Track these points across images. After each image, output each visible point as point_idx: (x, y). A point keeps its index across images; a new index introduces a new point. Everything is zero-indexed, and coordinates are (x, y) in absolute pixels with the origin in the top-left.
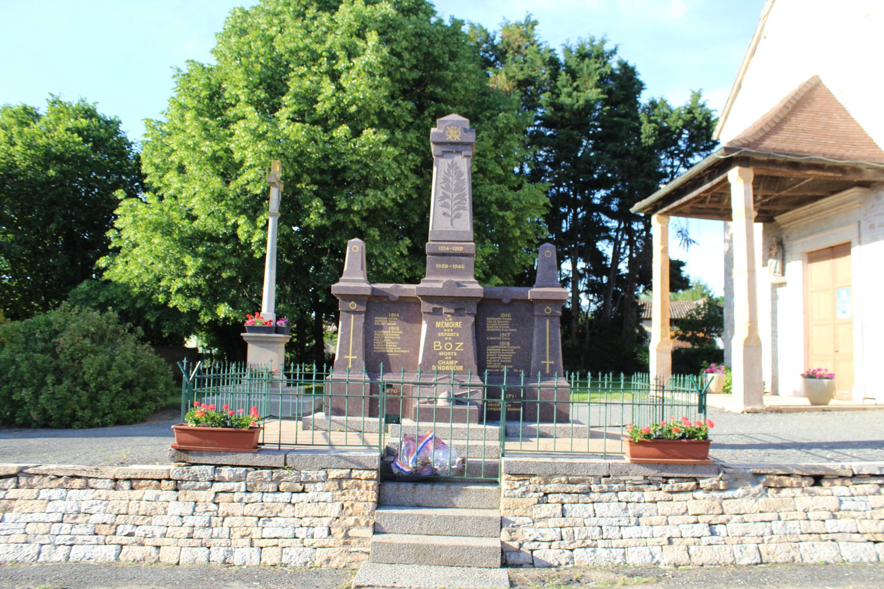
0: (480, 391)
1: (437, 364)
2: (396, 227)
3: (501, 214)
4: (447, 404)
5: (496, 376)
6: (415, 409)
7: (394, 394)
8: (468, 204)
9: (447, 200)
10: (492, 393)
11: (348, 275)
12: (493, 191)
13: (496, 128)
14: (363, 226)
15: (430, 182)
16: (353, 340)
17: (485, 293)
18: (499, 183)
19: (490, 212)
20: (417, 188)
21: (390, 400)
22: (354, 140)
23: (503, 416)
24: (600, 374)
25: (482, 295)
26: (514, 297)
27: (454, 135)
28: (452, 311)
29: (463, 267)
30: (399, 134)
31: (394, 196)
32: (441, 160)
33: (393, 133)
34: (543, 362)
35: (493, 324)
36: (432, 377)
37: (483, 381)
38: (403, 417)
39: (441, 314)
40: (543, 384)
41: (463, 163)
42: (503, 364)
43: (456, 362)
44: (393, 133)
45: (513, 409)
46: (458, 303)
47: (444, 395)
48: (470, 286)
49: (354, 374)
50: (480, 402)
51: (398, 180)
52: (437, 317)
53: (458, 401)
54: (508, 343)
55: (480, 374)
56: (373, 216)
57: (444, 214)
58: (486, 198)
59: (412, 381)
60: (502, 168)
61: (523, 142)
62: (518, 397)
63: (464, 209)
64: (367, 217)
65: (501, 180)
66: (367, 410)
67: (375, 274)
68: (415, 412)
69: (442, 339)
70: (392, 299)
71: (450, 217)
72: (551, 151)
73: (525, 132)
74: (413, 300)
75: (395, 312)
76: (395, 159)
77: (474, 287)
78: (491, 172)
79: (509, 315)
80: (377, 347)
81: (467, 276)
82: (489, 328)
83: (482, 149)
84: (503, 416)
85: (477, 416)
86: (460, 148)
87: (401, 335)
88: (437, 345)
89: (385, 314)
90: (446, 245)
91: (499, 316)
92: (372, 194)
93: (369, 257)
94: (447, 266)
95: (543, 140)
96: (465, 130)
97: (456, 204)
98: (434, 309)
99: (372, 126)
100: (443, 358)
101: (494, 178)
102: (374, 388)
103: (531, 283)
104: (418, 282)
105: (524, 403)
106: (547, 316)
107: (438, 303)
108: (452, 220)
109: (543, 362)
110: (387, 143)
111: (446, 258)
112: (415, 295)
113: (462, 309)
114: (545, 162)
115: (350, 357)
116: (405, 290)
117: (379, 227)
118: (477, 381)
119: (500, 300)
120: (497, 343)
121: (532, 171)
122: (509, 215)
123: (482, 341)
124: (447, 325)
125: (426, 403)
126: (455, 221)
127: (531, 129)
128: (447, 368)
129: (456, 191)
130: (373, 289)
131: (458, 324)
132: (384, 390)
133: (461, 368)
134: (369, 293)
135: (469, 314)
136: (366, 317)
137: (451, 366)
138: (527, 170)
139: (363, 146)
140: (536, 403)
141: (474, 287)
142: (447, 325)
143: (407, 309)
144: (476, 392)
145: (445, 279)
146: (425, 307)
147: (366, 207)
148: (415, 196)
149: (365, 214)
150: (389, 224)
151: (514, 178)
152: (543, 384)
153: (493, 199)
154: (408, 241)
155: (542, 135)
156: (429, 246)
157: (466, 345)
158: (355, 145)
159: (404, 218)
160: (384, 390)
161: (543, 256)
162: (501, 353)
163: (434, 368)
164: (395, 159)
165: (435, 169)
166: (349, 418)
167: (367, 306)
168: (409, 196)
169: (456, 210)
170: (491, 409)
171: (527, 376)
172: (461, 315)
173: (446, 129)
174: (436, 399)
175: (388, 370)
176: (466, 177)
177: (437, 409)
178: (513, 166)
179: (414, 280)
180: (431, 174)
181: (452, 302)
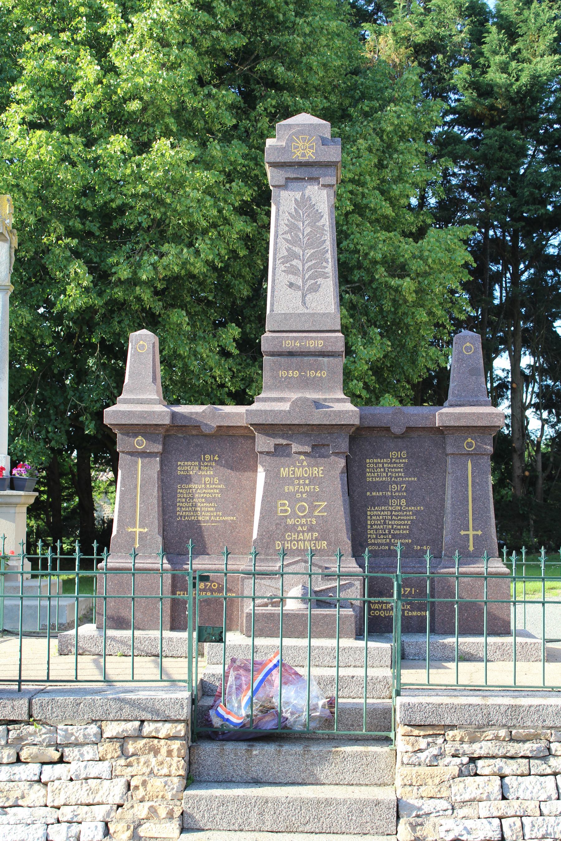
0: (358, 584)
2: (209, 304)
3: (394, 282)
4: (303, 606)
5: (382, 558)
6: (249, 615)
7: (212, 591)
8: (330, 268)
9: (295, 262)
10: (377, 588)
11: (131, 391)
12: (379, 244)
13: (380, 133)
14: (158, 307)
15: (267, 227)
16: (142, 502)
17: (361, 418)
18: (388, 229)
19: (373, 280)
20: (246, 239)
21: (207, 602)
22: (137, 157)
23: (397, 625)
25: (357, 422)
26: (412, 424)
27: (306, 151)
28: (308, 449)
29: (324, 374)
30: (215, 149)
31: (211, 257)
32: (284, 194)
33: (203, 144)
34: (462, 533)
35: (377, 470)
36: (276, 561)
37: (362, 566)
38: (229, 629)
39: (289, 455)
40: (462, 570)
41: (322, 198)
42: (394, 536)
43: (316, 534)
44: (203, 144)
45: (415, 613)
46: (316, 436)
47: (296, 591)
48: (337, 407)
49: (145, 557)
50: (357, 603)
51: (214, 226)
52: (283, 460)
53: (320, 600)
54: (403, 501)
55: (357, 554)
56: (172, 290)
57: (291, 285)
58: (367, 254)
59: (242, 568)
60: (392, 205)
61: (426, 154)
62: (422, 593)
63: (324, 276)
64: (164, 290)
65: (388, 225)
66: (167, 619)
67: (179, 384)
68: (248, 621)
69: (290, 497)
70: (207, 431)
71: (301, 293)
72: (472, 167)
73: (428, 135)
74: (242, 432)
75: (212, 453)
76: (208, 191)
77: (344, 409)
78: (374, 211)
79: (404, 454)
80: (182, 512)
81: (331, 389)
82: (370, 477)
83: (358, 171)
84: (397, 625)
85: (352, 626)
86: (315, 172)
88: (284, 506)
89: (196, 455)
90: (296, 339)
91: (387, 457)
92: (173, 252)
93: (167, 361)
94: (296, 374)
95: (459, 149)
96: (324, 141)
97: (310, 268)
98: (277, 446)
99: (167, 133)
100: (293, 528)
101: (377, 221)
102: (177, 584)
103: (440, 399)
104: (251, 403)
105: (433, 603)
106: (469, 454)
107: (283, 437)
108: (304, 296)
109: (462, 533)
110: (194, 163)
111: (294, 360)
112: (243, 423)
113: (324, 445)
114: (463, 187)
115: (138, 530)
116: (228, 415)
117: (183, 306)
118: (351, 566)
119: (388, 429)
120: (384, 501)
121: (440, 203)
122: (407, 284)
123: (358, 498)
124: (299, 472)
125: (266, 605)
126: (308, 296)
127: (438, 130)
128: (301, 545)
129: (310, 245)
130: (174, 415)
132: (194, 586)
133: (324, 544)
134: (167, 421)
135: (336, 454)
136: (162, 462)
137: (306, 541)
138: (432, 201)
139: (154, 168)
140: (453, 604)
141: (344, 409)
142: (299, 472)
143: (233, 448)
144: (351, 585)
145: (294, 396)
146: (263, 443)
147: (163, 274)
148: (242, 253)
149: (159, 286)
150: (200, 300)
151: (410, 217)
152: (462, 570)
153: (379, 257)
154: (234, 331)
155: (457, 139)
156: (267, 341)
157: (332, 507)
158: (138, 166)
159: (224, 288)
160: (194, 586)
161: (461, 352)
162: (392, 517)
163: (278, 545)
164: (208, 191)
165: (273, 209)
166: (137, 633)
167: (164, 445)
168: (234, 254)
169: (310, 278)
170: (377, 613)
171: (437, 556)
172: (323, 456)
173: (290, 140)
174: (283, 600)
175: (201, 550)
176: (326, 222)
177: (285, 615)
178: (408, 197)
179: (241, 398)
180: (268, 214)
181: (306, 434)
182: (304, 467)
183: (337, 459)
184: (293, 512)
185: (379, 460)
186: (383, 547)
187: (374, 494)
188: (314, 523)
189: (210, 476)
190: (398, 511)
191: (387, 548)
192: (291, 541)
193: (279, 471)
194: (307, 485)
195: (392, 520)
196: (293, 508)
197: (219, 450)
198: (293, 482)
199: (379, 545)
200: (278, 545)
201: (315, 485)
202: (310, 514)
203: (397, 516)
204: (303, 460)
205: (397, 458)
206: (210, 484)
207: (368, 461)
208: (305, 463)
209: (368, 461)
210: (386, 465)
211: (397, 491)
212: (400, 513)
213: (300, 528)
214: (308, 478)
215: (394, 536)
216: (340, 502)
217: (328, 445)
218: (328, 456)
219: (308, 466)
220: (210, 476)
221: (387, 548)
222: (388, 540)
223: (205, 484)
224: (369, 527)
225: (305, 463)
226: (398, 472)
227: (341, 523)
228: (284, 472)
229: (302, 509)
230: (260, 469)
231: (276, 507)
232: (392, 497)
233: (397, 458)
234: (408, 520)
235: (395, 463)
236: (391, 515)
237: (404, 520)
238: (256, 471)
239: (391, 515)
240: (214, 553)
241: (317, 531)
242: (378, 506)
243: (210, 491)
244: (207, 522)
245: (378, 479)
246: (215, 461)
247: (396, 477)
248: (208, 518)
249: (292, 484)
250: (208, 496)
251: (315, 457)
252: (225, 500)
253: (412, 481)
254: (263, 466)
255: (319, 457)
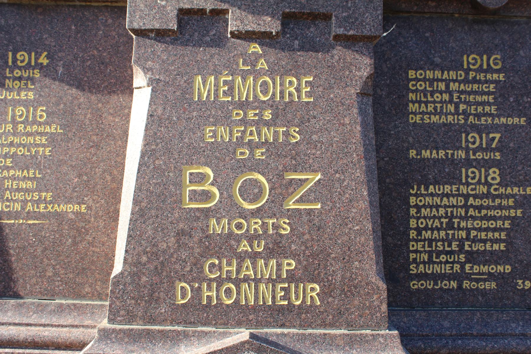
1: (197, 276)
24: (439, 282)
28: (271, 25)
39: (219, 41)
42: (473, 257)
43: (290, 264)
54: (494, 173)
69: (221, 157)
75: (33, 47)
82: (418, 113)
87: (52, 139)
88: (200, 183)
91: (458, 66)
100: (225, 246)
120: (449, 172)
124: (245, 88)
131: (296, 87)
137: (263, 281)
142: (245, 88)
157: (331, 188)
163: (183, 293)
182: (257, 74)
183: (349, 55)
184: (228, 198)
185: (438, 74)
186: (445, 284)
187: (426, 154)
188: (286, 230)
189: (26, 104)
190: (482, 196)
191: (454, 284)
192: (220, 282)
193: (190, 83)
194: (267, 124)
195: (466, 218)
196: (226, 188)
197: (50, 41)
198: (228, 116)
199: (436, 277)
200: (183, 293)
201: (288, 124)
202: (274, 208)
203: (479, 208)
204: (257, 57)
205: (480, 70)
206: (26, 122)
207: (412, 74)
208: (262, 65)
209: (412, 74)
210: (454, 86)
211: (480, 148)
212: (486, 202)
213: (244, 247)
214: (271, 104)
215: (473, 257)
216: (359, 174)
217: (327, 17)
218: (326, 48)
219: (271, 73)
220: (26, 104)
221: (454, 284)
222: (457, 267)
223: (14, 122)
224: (413, 234)
225: (262, 65)
226: (483, 104)
227: (361, 233)
228: (203, 87)
229: (251, 191)
230: (140, 79)
231: (179, 185)
232: (468, 163)
233: (480, 70)
234: (504, 218)
235: (475, 81)
236: (466, 207)
237: (494, 218)
238: (128, 89)
239: (466, 207)
240: (31, 294)
241: (294, 255)
242: (436, 183)
243: (25, 140)
244: (16, 215)
245: (435, 119)
246: (41, 67)
247: (478, 116)
248: (18, 207)
249: (225, 119)
250: (21, 151)
251: (291, 49)
252: (61, 163)
253: (515, 126)
254: (146, 70)
255: (302, 48)
